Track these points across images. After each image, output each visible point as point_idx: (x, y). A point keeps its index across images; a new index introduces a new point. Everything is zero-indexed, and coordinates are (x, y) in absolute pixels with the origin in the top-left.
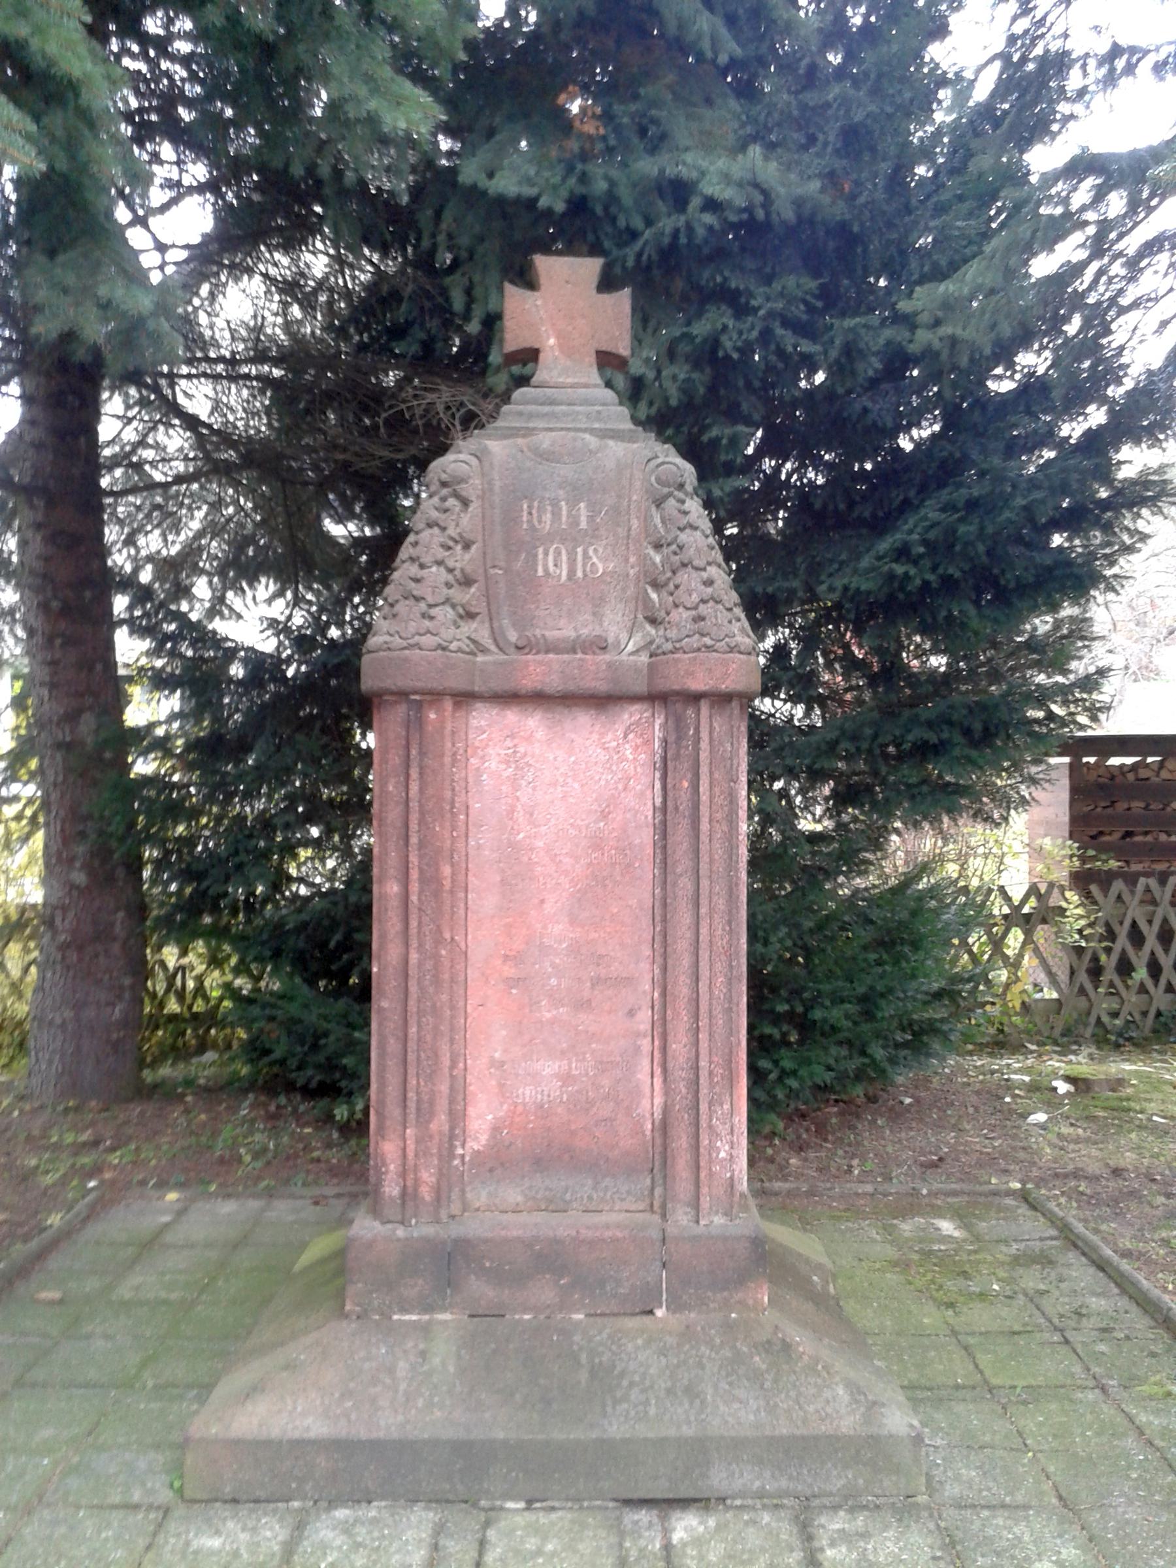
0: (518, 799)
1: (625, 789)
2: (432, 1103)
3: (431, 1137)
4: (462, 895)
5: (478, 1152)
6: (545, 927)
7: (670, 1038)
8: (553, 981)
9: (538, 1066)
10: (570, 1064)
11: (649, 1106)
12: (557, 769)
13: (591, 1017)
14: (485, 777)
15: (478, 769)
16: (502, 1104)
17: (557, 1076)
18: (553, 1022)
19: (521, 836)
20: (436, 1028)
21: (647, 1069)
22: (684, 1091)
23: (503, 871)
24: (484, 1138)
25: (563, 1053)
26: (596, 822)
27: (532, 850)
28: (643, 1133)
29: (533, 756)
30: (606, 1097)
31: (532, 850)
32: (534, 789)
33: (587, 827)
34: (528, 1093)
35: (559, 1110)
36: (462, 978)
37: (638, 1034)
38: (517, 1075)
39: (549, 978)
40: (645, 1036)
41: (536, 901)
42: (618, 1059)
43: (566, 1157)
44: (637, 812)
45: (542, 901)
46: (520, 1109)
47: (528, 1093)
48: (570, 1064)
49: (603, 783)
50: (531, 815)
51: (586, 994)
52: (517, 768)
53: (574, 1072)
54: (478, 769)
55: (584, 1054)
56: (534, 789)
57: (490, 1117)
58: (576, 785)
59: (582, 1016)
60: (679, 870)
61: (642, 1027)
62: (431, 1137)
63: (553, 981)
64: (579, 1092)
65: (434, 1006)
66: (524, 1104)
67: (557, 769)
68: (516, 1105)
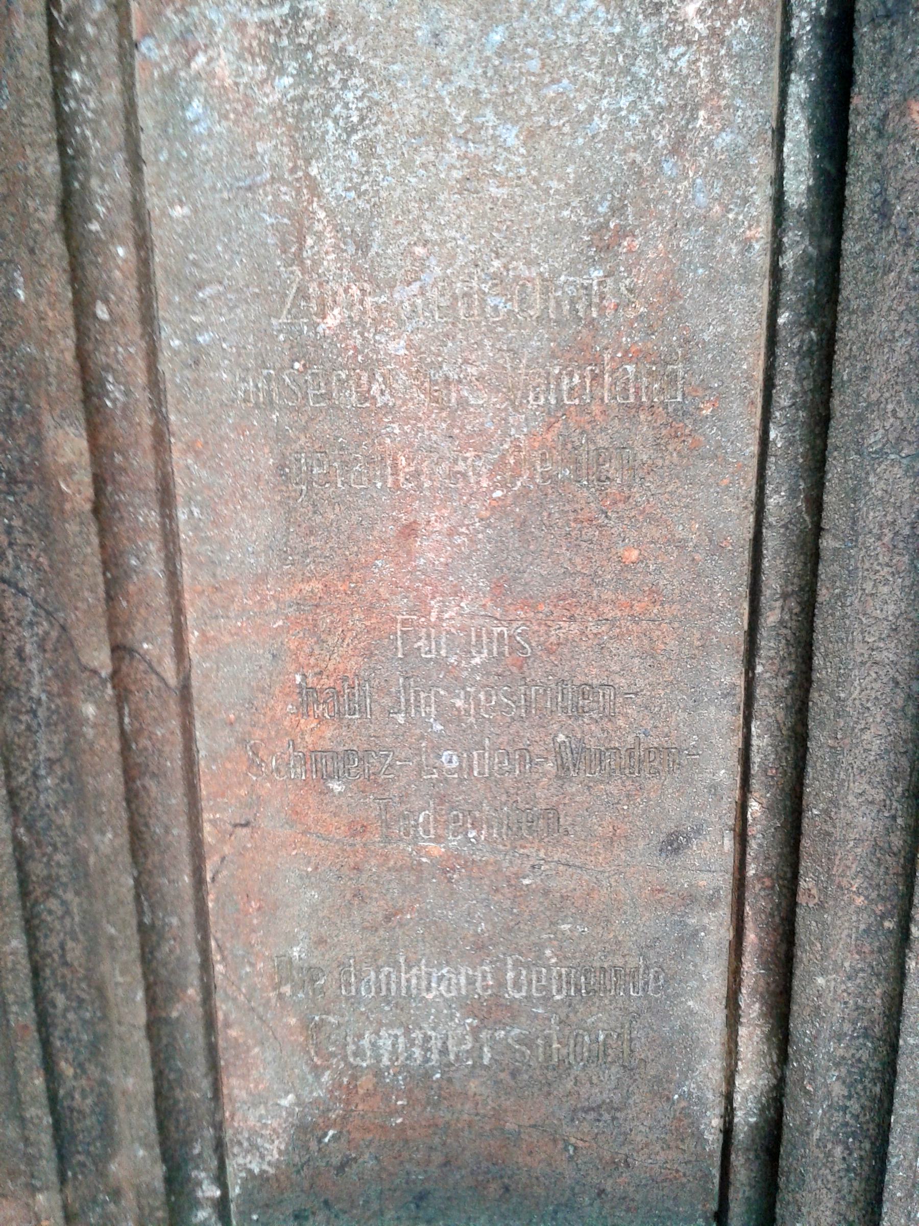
0: (314, 188)
1: (677, 147)
2: (106, 1116)
3: (116, 1194)
4: (151, 516)
5: (263, 1178)
6: (420, 607)
7: (804, 957)
8: (449, 759)
9: (413, 977)
10: (499, 974)
11: (716, 1077)
12: (445, 75)
13: (558, 854)
14: (196, 107)
15: (169, 81)
16: (317, 1070)
17: (469, 1006)
18: (445, 868)
19: (333, 320)
20: (91, 924)
21: (718, 986)
22: (838, 1090)
23: (281, 437)
24: (274, 1150)
25: (480, 947)
26: (573, 269)
27: (369, 366)
28: (699, 1137)
29: (358, 29)
30: (599, 1056)
31: (369, 366)
32: (368, 150)
33: (548, 284)
34: (385, 1043)
35: (473, 1086)
36: (174, 762)
37: (690, 899)
38: (353, 1001)
39: (436, 751)
40: (712, 903)
41: (391, 529)
42: (635, 961)
43: (494, 1189)
44: (715, 228)
45: (409, 531)
46: (366, 1082)
47: (385, 1043)
48: (499, 974)
49: (600, 124)
50: (363, 246)
51: (544, 795)
52: (304, 73)
53: (512, 993)
54: (169, 81)
55: (540, 947)
56: (368, 150)
57: (288, 1100)
58: (511, 136)
59: (534, 851)
60: (873, 440)
61: (704, 881)
62: (116, 1194)
63: (449, 759)
64: (527, 1041)
65: (79, 860)
66: (378, 1073)
67: (445, 75)
68: (355, 1073)
